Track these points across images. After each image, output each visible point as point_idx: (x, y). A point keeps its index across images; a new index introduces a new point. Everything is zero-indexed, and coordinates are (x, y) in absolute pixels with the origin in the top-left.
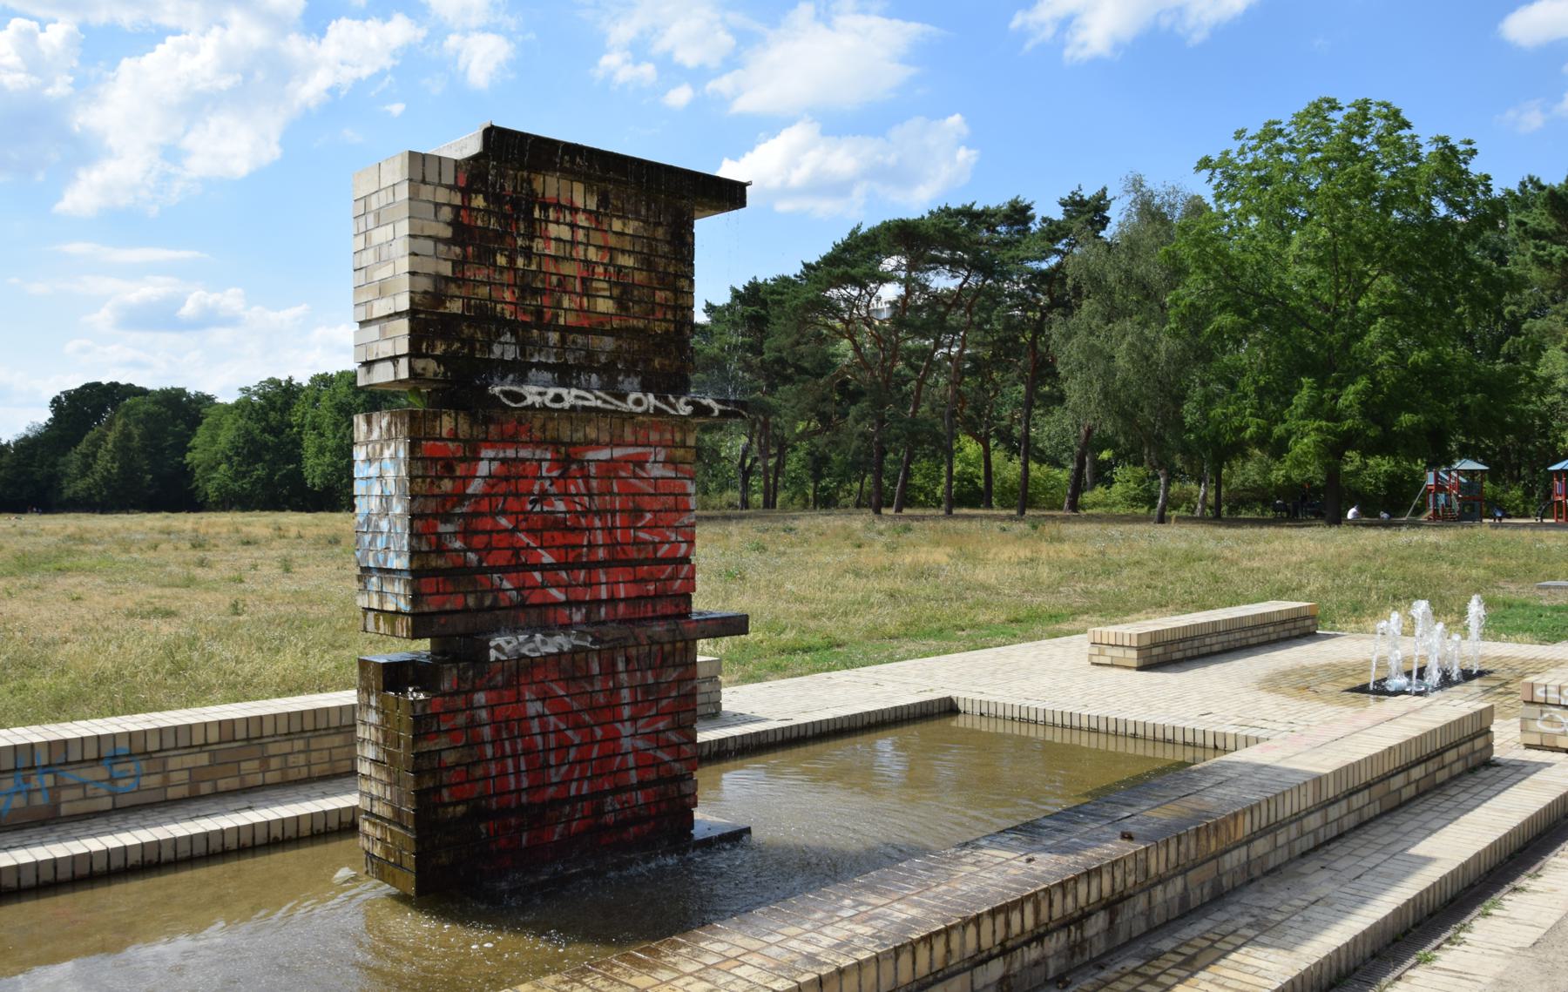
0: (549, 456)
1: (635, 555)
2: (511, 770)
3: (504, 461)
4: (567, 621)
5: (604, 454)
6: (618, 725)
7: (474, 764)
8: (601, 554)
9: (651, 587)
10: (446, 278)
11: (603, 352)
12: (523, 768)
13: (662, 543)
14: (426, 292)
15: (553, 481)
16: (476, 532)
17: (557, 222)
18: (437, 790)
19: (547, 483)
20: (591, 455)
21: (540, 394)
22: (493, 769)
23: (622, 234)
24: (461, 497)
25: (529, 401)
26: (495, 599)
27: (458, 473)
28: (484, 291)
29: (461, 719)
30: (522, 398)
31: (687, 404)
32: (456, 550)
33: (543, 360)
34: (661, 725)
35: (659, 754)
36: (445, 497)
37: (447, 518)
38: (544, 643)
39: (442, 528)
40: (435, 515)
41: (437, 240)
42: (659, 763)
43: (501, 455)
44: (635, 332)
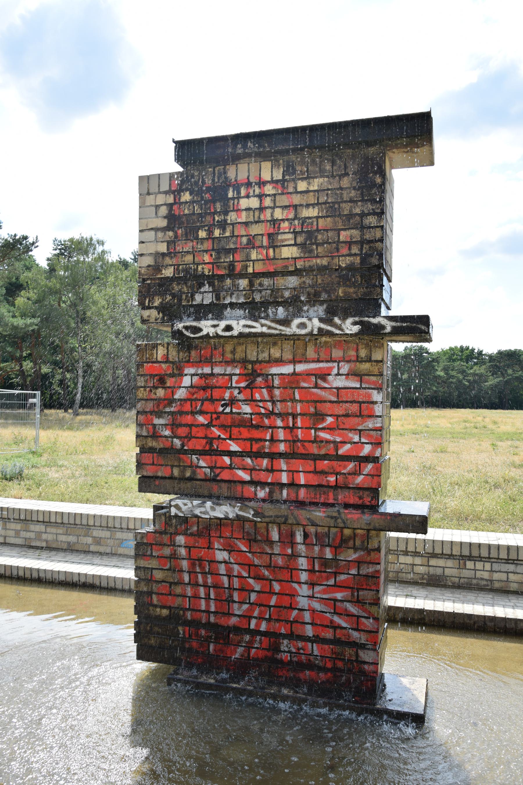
0: (237, 371)
1: (316, 451)
2: (202, 595)
3: (203, 376)
4: (252, 496)
5: (287, 369)
6: (296, 586)
7: (176, 584)
8: (282, 447)
9: (332, 479)
10: (163, 255)
11: (287, 289)
12: (212, 596)
13: (344, 443)
14: (149, 266)
15: (241, 390)
16: (180, 425)
17: (248, 196)
18: (150, 593)
19: (236, 392)
20: (275, 370)
21: (214, 326)
22: (189, 592)
23: (307, 192)
24: (170, 401)
25: (204, 332)
26: (194, 473)
27: (168, 385)
28: (189, 258)
29: (167, 551)
30: (200, 330)
31: (355, 323)
32: (166, 437)
33: (234, 300)
34: (339, 596)
35: (336, 619)
36: (159, 401)
37: (159, 414)
38: (213, 509)
39: (156, 421)
40: (151, 412)
41: (156, 230)
42: (336, 627)
43: (200, 371)
44: (322, 269)
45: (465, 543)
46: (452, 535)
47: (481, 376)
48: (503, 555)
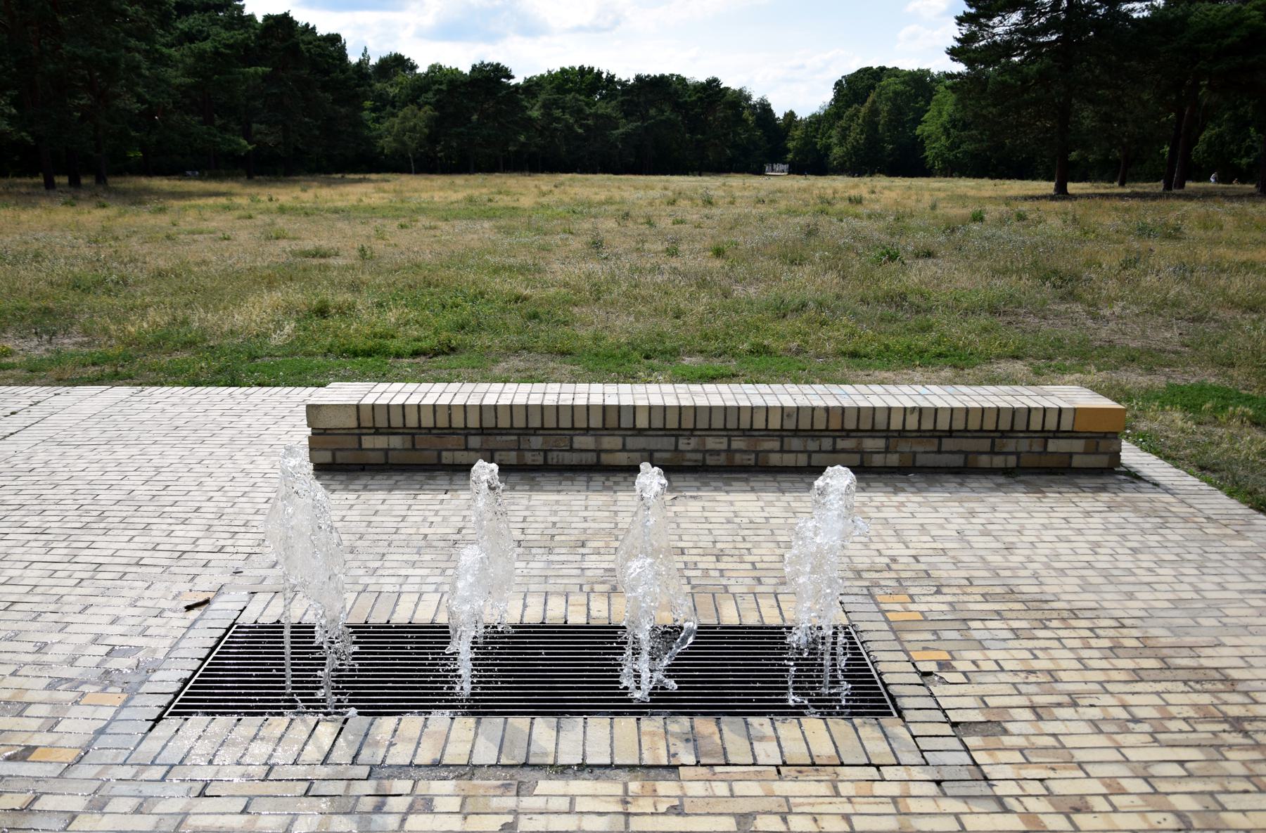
45: (775, 407)
46: (662, 394)
47: (608, 117)
48: (718, 423)
